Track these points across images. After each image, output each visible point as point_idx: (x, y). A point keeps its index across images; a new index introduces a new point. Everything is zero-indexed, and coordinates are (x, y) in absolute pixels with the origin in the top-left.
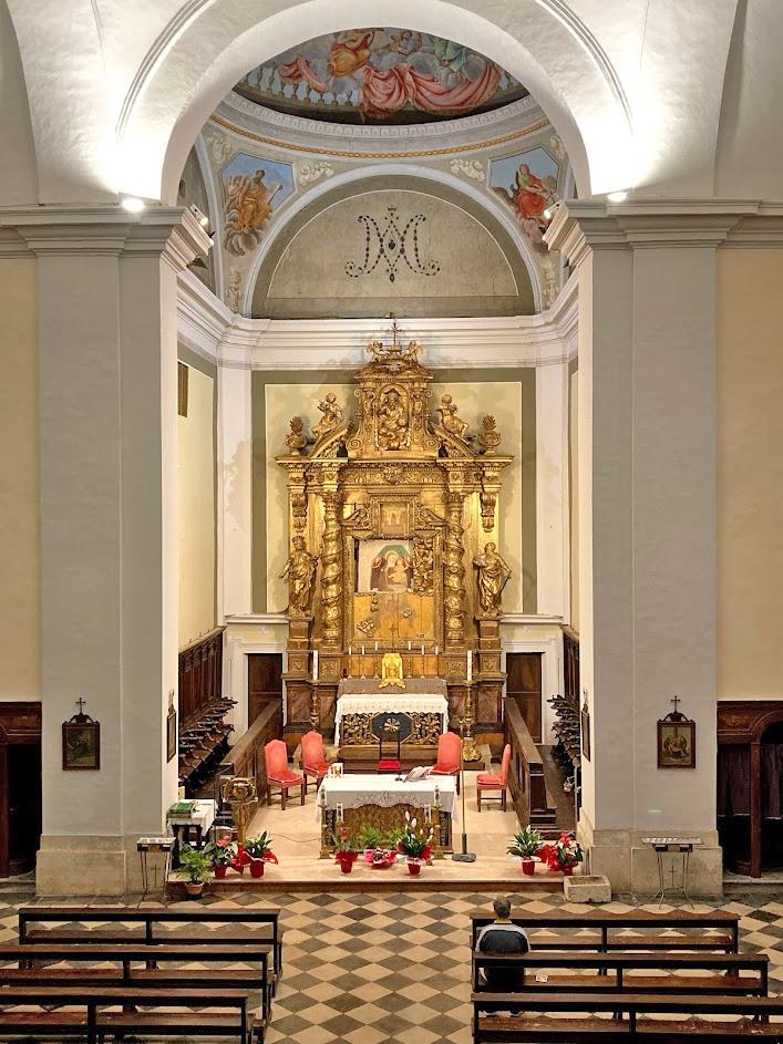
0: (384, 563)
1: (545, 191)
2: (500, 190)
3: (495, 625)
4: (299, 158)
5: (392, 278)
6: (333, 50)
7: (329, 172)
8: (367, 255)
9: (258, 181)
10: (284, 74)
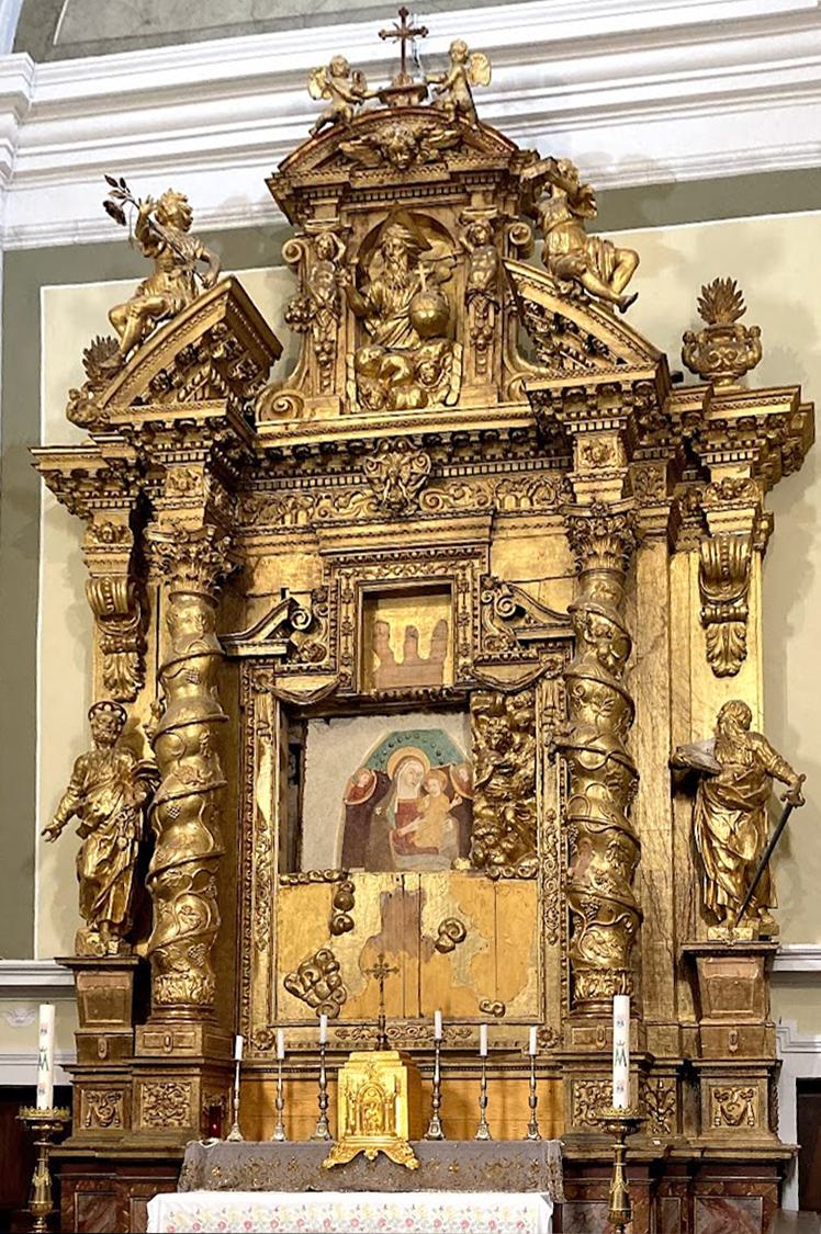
0: (383, 786)
3: (750, 970)
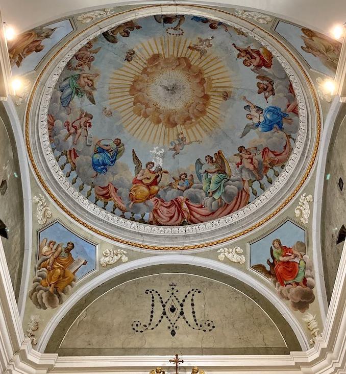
1: (296, 256)
2: (259, 267)
4: (102, 242)
5: (173, 333)
6: (134, 183)
7: (125, 258)
8: (152, 316)
9: (68, 251)
10: (99, 193)
